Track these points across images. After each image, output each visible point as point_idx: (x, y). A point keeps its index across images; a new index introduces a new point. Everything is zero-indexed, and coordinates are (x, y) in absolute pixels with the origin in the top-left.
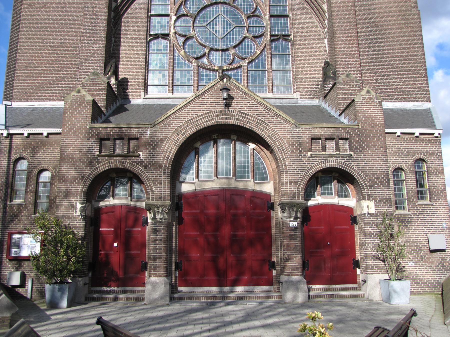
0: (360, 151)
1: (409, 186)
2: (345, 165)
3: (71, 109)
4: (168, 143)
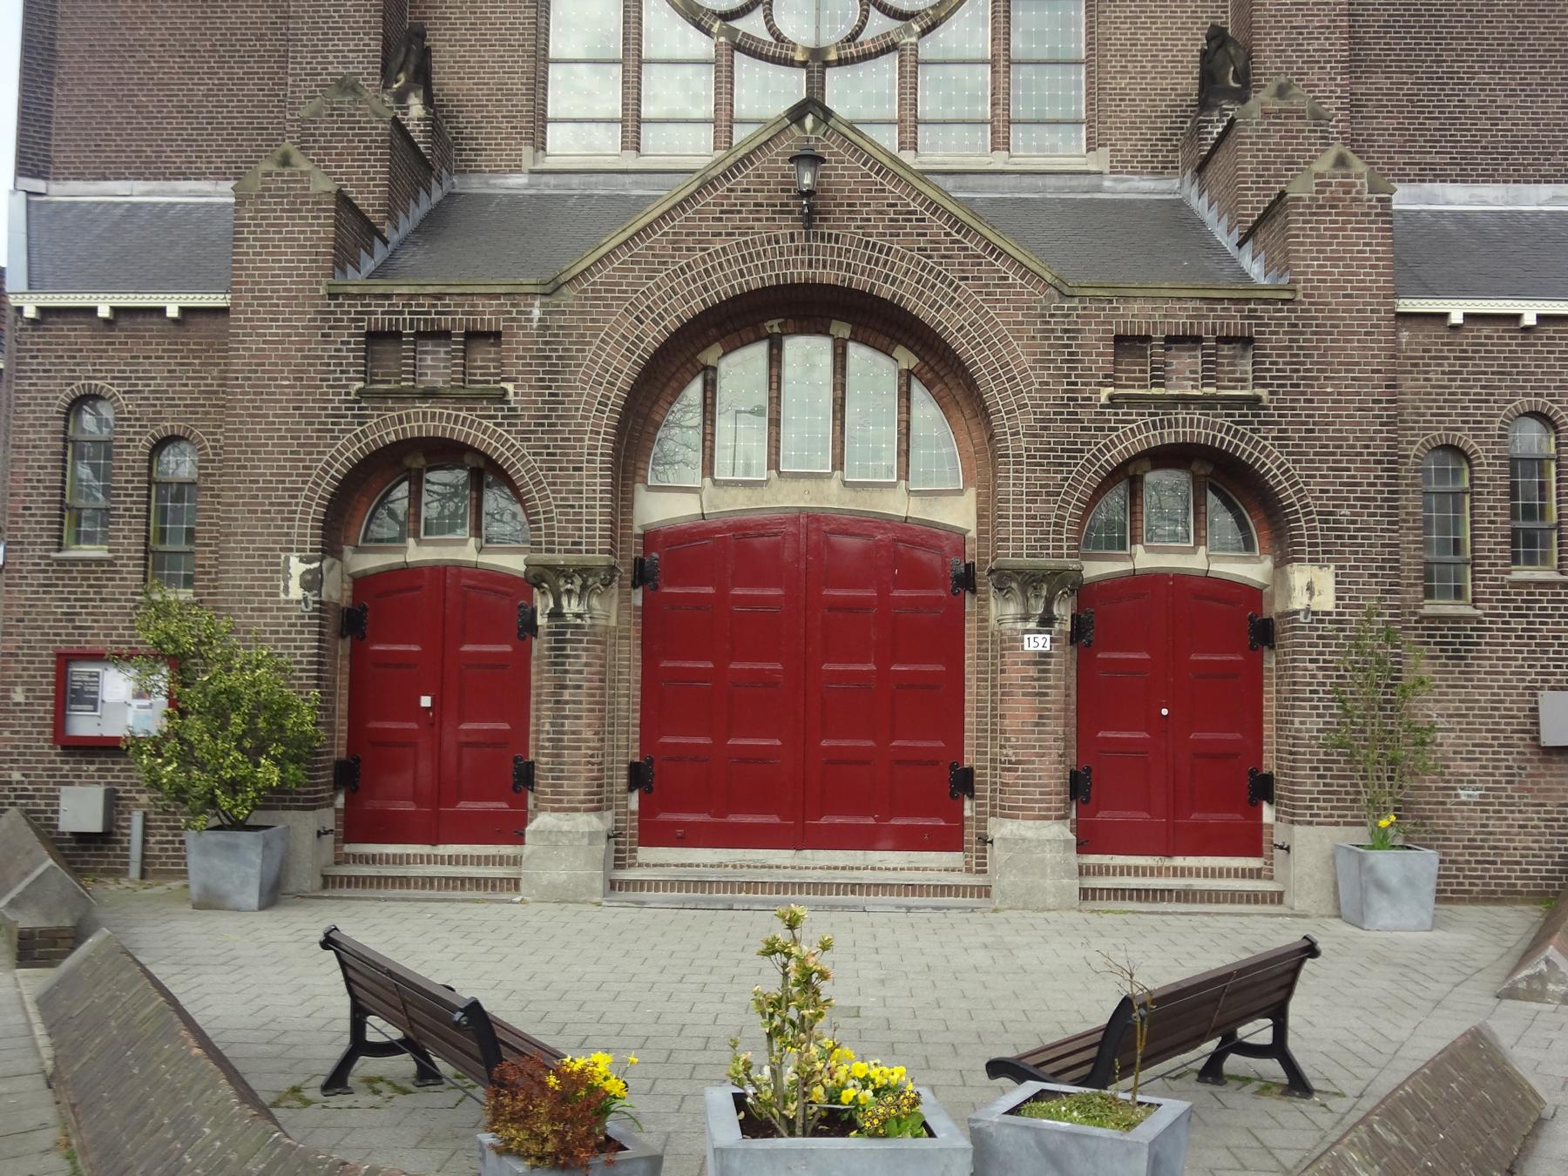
0: (1292, 386)
1: (1482, 515)
2: (1234, 437)
3: (260, 225)
4: (603, 350)
